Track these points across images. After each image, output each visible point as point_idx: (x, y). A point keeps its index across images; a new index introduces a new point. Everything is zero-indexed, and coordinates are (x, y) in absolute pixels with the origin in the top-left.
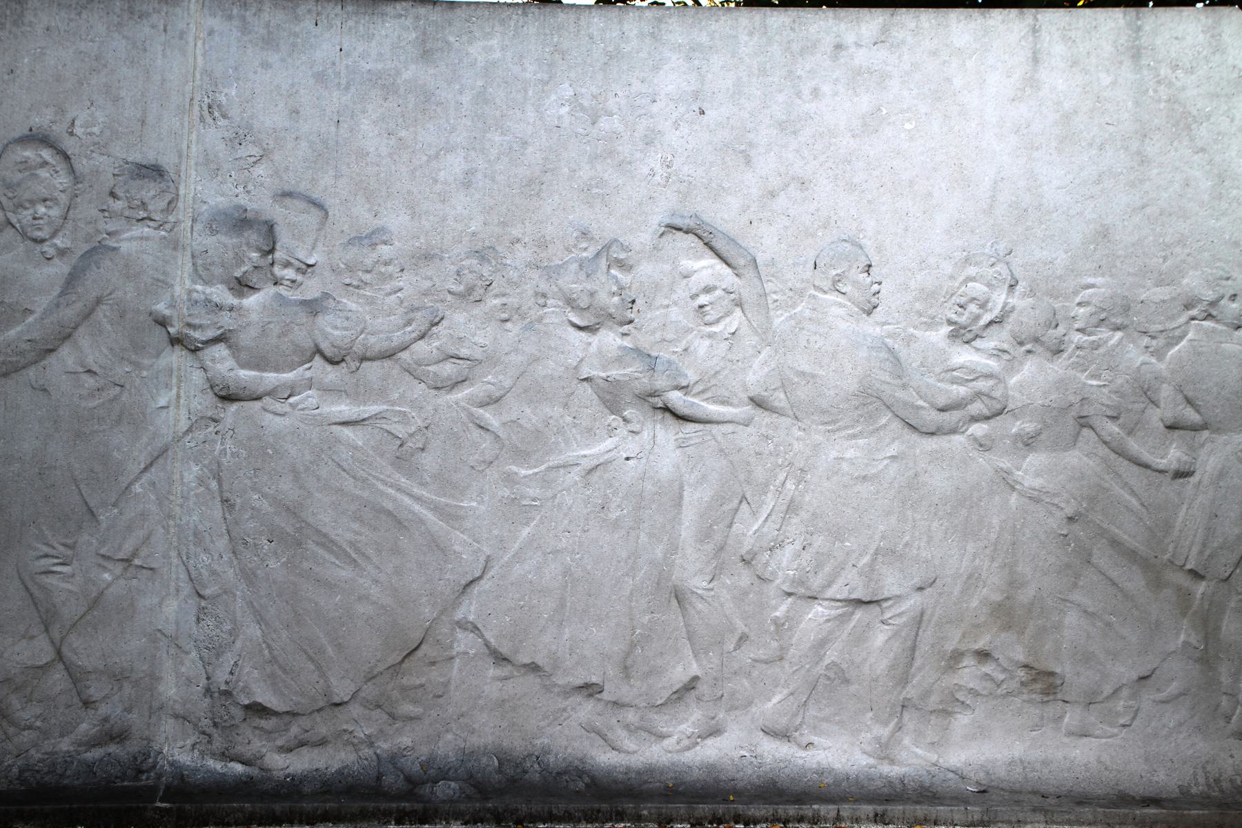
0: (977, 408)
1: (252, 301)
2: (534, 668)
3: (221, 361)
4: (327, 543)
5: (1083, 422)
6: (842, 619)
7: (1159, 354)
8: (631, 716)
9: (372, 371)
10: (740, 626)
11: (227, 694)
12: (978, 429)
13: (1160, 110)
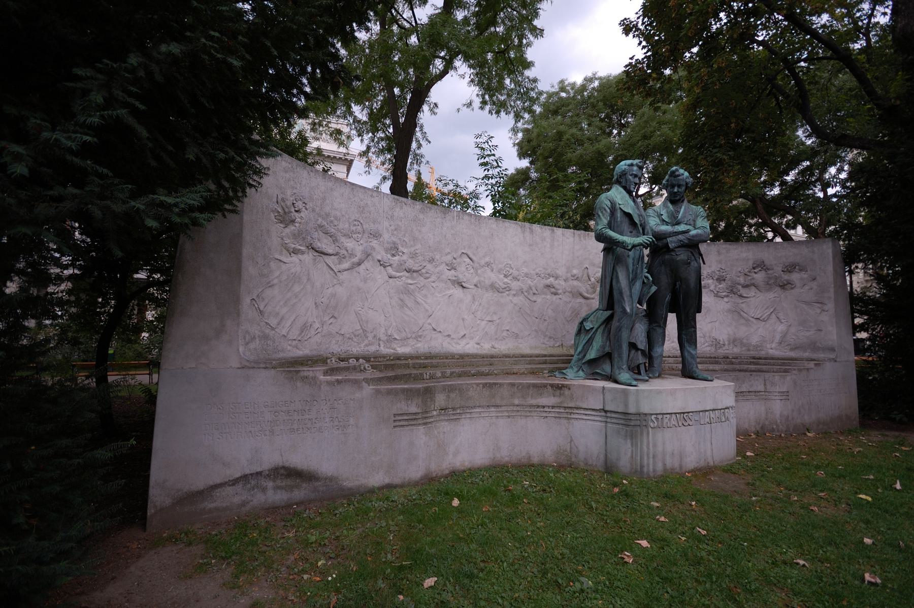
0: (507, 289)
1: (395, 258)
2: (440, 332)
5: (522, 292)
8: (455, 341)
9: (415, 274)
12: (507, 292)
13: (92, 347)
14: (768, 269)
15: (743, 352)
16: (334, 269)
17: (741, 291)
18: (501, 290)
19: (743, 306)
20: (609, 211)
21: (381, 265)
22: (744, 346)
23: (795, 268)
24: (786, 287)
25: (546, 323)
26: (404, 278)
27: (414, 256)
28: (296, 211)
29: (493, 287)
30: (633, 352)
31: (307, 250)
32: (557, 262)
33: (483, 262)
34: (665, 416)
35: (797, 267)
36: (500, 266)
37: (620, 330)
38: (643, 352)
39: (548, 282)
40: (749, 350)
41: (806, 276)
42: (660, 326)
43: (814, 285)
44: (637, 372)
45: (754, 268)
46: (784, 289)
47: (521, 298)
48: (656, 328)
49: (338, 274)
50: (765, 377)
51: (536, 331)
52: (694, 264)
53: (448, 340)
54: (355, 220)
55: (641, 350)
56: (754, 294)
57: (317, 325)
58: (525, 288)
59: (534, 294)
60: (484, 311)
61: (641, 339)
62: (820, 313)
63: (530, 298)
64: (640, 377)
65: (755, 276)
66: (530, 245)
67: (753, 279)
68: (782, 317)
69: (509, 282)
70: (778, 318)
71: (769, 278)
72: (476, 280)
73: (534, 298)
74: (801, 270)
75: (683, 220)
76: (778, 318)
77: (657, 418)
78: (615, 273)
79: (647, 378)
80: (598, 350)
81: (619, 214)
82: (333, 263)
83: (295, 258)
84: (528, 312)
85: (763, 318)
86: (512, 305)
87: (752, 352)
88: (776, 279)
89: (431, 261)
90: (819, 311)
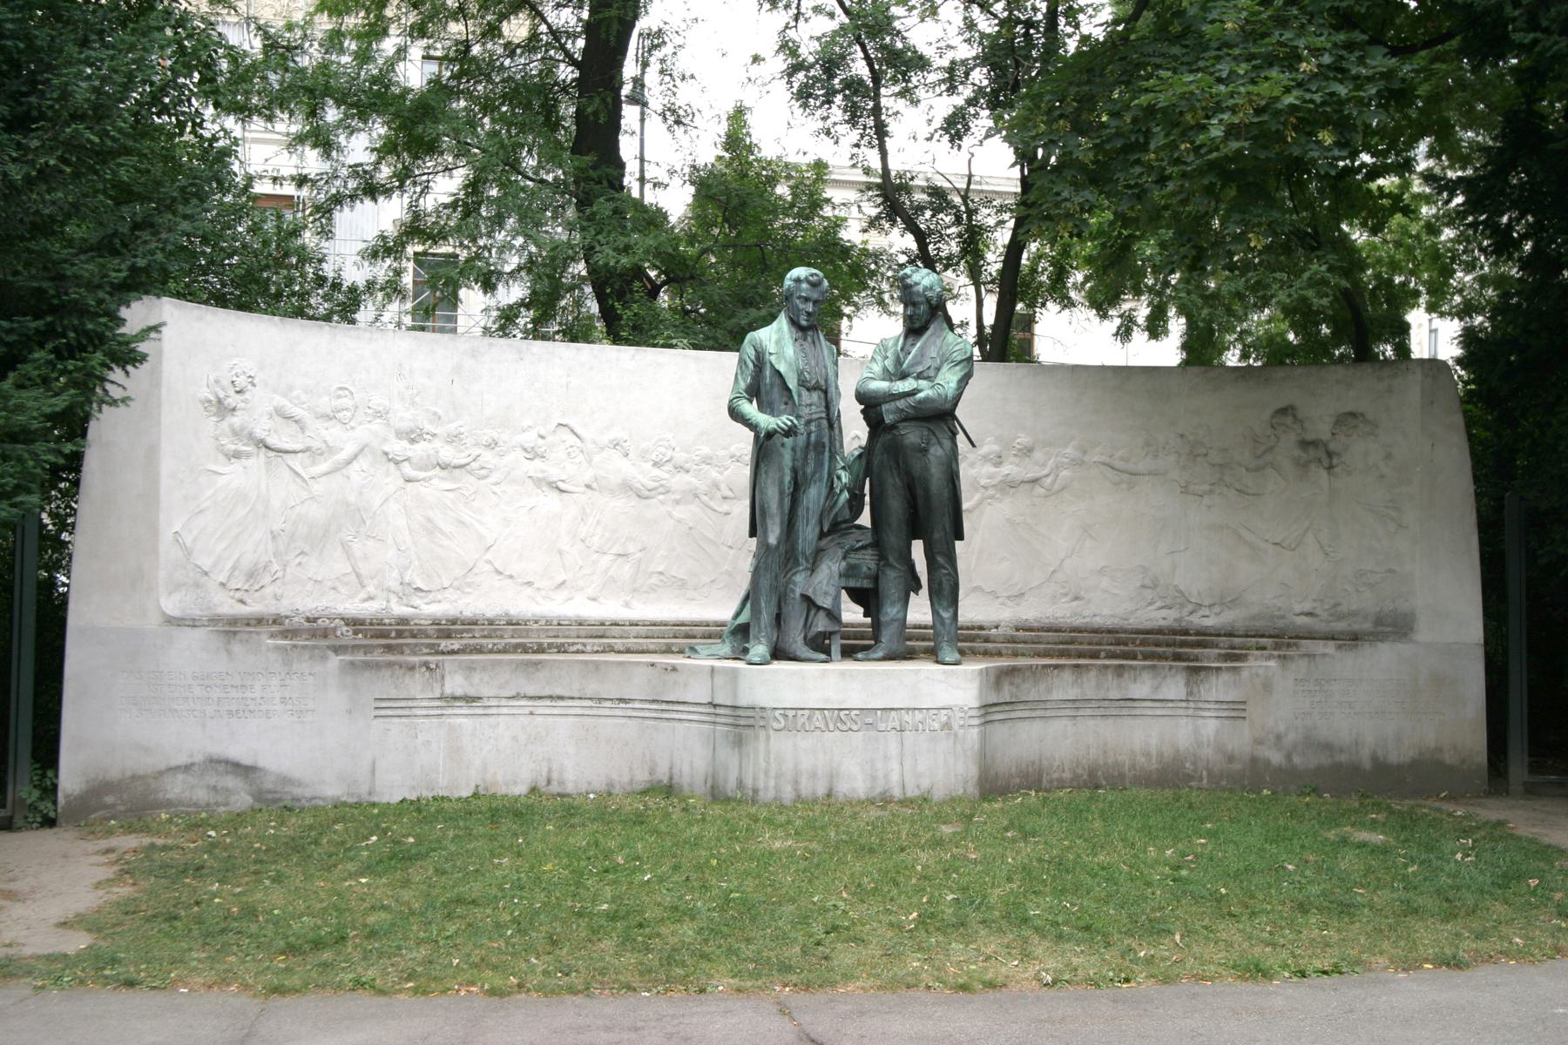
0: (661, 490)
1: (416, 446)
2: (511, 577)
3: (407, 469)
4: (442, 532)
5: (696, 496)
6: (615, 560)
7: (721, 473)
8: (543, 593)
10: (581, 563)
11: (409, 584)
12: (661, 497)
16: (303, 474)
20: (751, 366)
21: (390, 460)
26: (435, 481)
27: (454, 439)
28: (238, 392)
29: (627, 488)
31: (256, 450)
33: (605, 439)
34: (800, 712)
47: (694, 508)
49: (311, 482)
52: (936, 452)
53: (528, 591)
54: (341, 389)
55: (825, 609)
57: (275, 567)
58: (702, 486)
60: (607, 534)
69: (666, 476)
72: (587, 477)
73: (725, 507)
75: (912, 370)
77: (785, 716)
81: (768, 372)
82: (301, 464)
83: (237, 466)
89: (492, 445)
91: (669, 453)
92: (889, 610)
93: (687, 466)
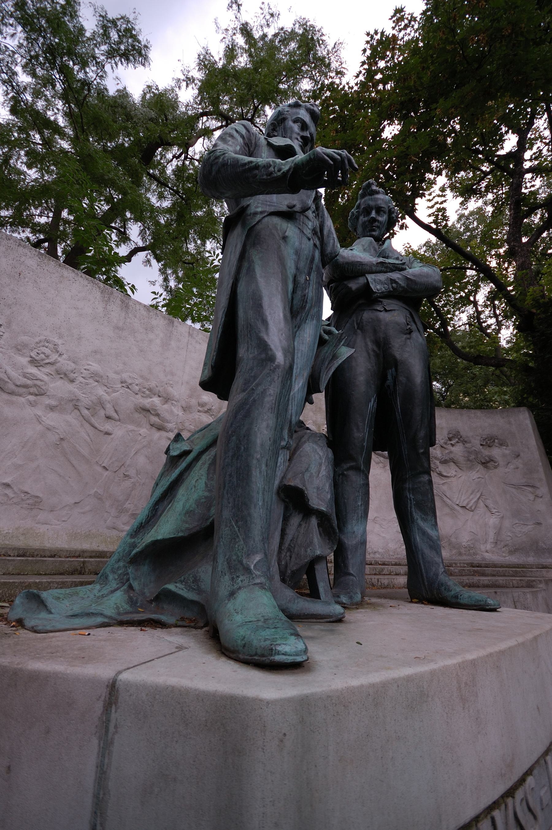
5: (76, 407)
12: (31, 398)
14: (466, 442)
15: (454, 558)
17: (439, 467)
18: (13, 387)
19: (445, 488)
22: (454, 547)
23: (494, 441)
24: (488, 465)
25: (127, 484)
30: (295, 520)
32: (172, 374)
35: (496, 441)
36: (25, 338)
37: (248, 414)
38: (322, 517)
39: (147, 402)
40: (460, 554)
41: (507, 452)
42: (357, 469)
43: (519, 462)
44: (308, 592)
45: (450, 439)
46: (486, 467)
47: (72, 418)
48: (351, 473)
50: (513, 597)
51: (98, 497)
56: (454, 473)
58: (85, 400)
59: (108, 417)
61: (317, 482)
62: (534, 501)
63: (97, 425)
64: (316, 607)
65: (453, 449)
66: (117, 328)
67: (451, 452)
68: (491, 506)
69: (46, 378)
70: (487, 506)
71: (469, 452)
73: (107, 427)
74: (501, 445)
76: (487, 506)
78: (246, 264)
79: (338, 609)
80: (189, 513)
84: (85, 451)
85: (470, 505)
86: (39, 428)
87: (465, 557)
88: (477, 454)
90: (532, 497)
91: (54, 357)
92: (355, 529)
93: (72, 375)
